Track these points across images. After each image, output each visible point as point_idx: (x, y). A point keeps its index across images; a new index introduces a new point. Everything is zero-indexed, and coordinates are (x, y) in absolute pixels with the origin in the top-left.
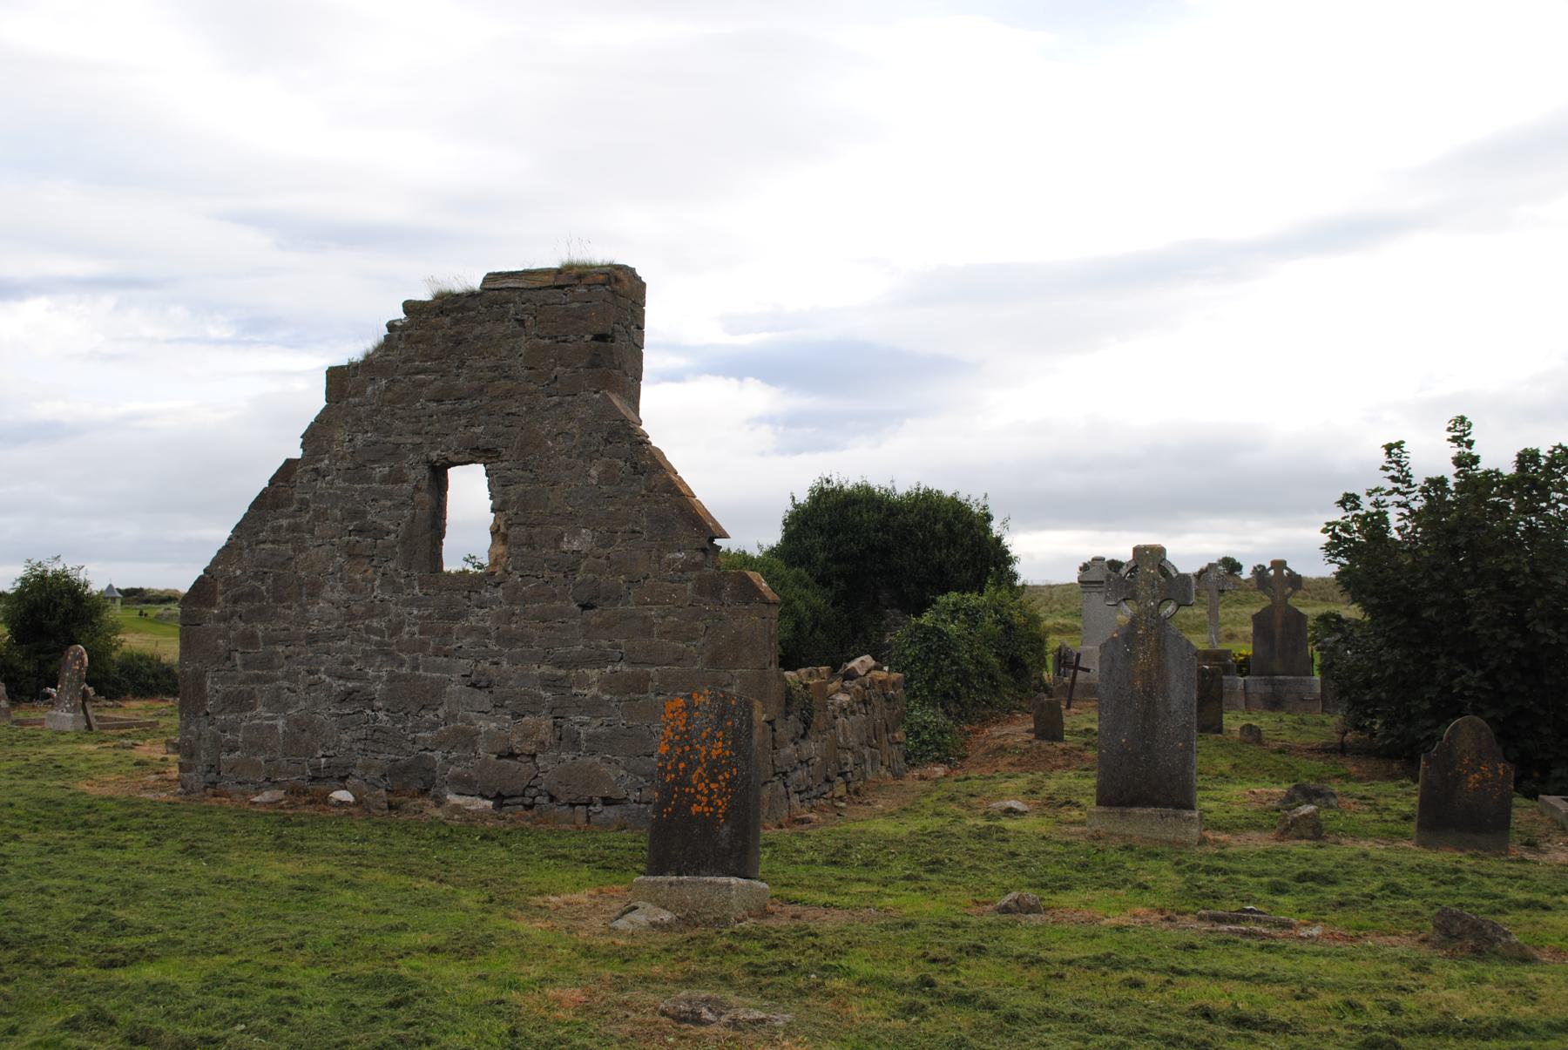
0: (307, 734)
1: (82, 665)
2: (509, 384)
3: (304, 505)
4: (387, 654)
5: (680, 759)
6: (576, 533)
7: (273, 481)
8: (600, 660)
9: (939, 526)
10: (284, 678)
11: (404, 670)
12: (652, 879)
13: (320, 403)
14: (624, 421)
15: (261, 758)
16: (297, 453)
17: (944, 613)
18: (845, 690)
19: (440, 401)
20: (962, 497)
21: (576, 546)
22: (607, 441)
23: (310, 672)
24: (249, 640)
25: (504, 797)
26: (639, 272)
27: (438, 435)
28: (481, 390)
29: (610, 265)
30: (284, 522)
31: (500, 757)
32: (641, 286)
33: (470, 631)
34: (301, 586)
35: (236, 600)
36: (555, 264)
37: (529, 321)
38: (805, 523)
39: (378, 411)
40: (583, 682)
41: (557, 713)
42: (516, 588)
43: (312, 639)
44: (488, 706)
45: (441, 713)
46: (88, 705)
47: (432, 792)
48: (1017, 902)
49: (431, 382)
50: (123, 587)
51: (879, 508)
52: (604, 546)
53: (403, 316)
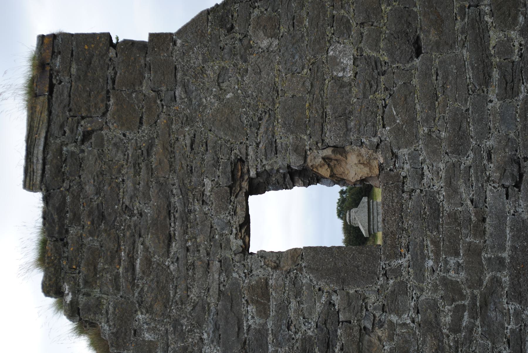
2: (158, 149)
4: (485, 304)
6: (334, 62)
8: (479, 33)
11: (506, 279)
19: (170, 238)
21: (348, 61)
28: (162, 186)
33: (453, 191)
37: (87, 125)
40: (505, 48)
42: (398, 131)
49: (146, 249)
52: (349, 28)
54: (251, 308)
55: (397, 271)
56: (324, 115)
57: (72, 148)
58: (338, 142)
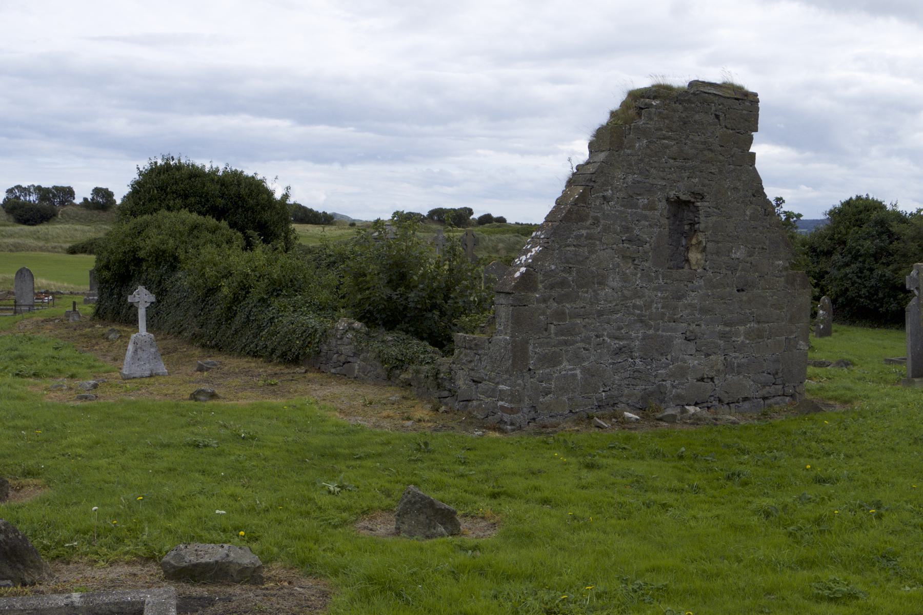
2: (711, 155)
4: (642, 321)
49: (672, 146)
54: (646, 201)
55: (657, 278)
56: (718, 242)
57: (713, 108)
58: (708, 249)
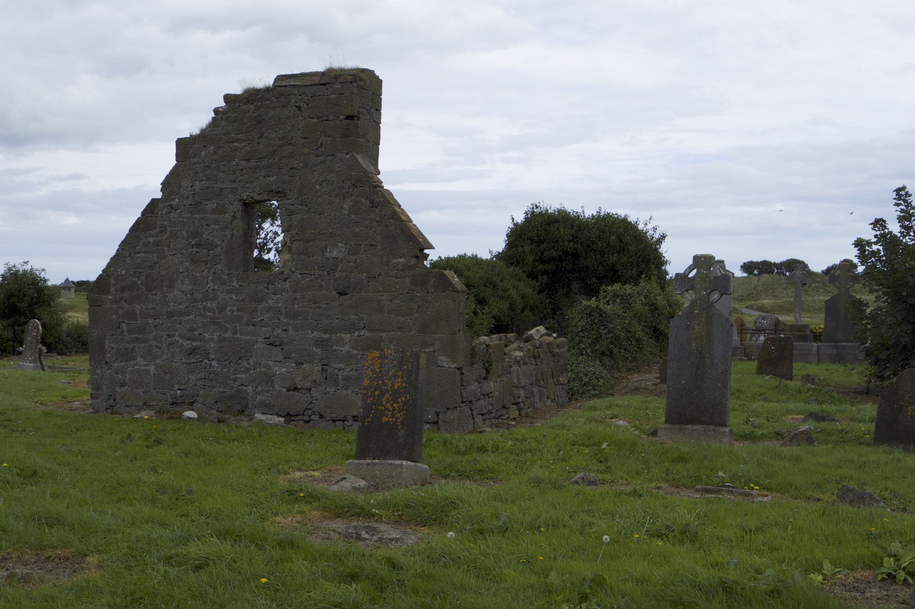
0: (168, 375)
1: (38, 332)
3: (163, 229)
5: (376, 389)
7: (143, 213)
9: (613, 237)
10: (153, 340)
11: (228, 335)
12: (357, 461)
13: (173, 162)
14: (365, 172)
15: (140, 391)
16: (159, 195)
17: (609, 301)
18: (520, 349)
19: (248, 160)
20: (632, 219)
21: (335, 254)
22: (355, 186)
23: (169, 336)
24: (131, 315)
25: (292, 416)
26: (377, 73)
27: (247, 183)
29: (357, 69)
30: (151, 240)
31: (288, 390)
32: (379, 82)
33: (269, 309)
34: (162, 281)
35: (123, 290)
36: (320, 68)
38: (521, 237)
39: (209, 167)
41: (323, 362)
43: (170, 315)
44: (280, 358)
45: (251, 362)
46: (42, 358)
47: (247, 412)
48: (583, 479)
49: (242, 148)
50: (76, 280)
51: (572, 226)
52: (353, 255)
53: (223, 104)
